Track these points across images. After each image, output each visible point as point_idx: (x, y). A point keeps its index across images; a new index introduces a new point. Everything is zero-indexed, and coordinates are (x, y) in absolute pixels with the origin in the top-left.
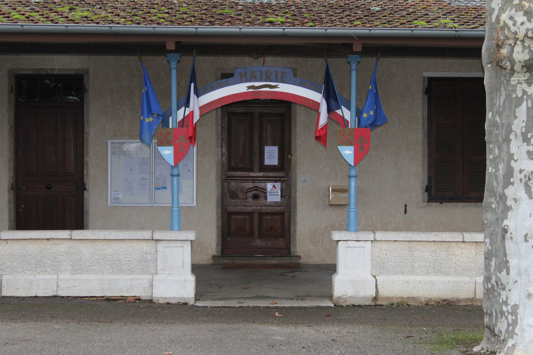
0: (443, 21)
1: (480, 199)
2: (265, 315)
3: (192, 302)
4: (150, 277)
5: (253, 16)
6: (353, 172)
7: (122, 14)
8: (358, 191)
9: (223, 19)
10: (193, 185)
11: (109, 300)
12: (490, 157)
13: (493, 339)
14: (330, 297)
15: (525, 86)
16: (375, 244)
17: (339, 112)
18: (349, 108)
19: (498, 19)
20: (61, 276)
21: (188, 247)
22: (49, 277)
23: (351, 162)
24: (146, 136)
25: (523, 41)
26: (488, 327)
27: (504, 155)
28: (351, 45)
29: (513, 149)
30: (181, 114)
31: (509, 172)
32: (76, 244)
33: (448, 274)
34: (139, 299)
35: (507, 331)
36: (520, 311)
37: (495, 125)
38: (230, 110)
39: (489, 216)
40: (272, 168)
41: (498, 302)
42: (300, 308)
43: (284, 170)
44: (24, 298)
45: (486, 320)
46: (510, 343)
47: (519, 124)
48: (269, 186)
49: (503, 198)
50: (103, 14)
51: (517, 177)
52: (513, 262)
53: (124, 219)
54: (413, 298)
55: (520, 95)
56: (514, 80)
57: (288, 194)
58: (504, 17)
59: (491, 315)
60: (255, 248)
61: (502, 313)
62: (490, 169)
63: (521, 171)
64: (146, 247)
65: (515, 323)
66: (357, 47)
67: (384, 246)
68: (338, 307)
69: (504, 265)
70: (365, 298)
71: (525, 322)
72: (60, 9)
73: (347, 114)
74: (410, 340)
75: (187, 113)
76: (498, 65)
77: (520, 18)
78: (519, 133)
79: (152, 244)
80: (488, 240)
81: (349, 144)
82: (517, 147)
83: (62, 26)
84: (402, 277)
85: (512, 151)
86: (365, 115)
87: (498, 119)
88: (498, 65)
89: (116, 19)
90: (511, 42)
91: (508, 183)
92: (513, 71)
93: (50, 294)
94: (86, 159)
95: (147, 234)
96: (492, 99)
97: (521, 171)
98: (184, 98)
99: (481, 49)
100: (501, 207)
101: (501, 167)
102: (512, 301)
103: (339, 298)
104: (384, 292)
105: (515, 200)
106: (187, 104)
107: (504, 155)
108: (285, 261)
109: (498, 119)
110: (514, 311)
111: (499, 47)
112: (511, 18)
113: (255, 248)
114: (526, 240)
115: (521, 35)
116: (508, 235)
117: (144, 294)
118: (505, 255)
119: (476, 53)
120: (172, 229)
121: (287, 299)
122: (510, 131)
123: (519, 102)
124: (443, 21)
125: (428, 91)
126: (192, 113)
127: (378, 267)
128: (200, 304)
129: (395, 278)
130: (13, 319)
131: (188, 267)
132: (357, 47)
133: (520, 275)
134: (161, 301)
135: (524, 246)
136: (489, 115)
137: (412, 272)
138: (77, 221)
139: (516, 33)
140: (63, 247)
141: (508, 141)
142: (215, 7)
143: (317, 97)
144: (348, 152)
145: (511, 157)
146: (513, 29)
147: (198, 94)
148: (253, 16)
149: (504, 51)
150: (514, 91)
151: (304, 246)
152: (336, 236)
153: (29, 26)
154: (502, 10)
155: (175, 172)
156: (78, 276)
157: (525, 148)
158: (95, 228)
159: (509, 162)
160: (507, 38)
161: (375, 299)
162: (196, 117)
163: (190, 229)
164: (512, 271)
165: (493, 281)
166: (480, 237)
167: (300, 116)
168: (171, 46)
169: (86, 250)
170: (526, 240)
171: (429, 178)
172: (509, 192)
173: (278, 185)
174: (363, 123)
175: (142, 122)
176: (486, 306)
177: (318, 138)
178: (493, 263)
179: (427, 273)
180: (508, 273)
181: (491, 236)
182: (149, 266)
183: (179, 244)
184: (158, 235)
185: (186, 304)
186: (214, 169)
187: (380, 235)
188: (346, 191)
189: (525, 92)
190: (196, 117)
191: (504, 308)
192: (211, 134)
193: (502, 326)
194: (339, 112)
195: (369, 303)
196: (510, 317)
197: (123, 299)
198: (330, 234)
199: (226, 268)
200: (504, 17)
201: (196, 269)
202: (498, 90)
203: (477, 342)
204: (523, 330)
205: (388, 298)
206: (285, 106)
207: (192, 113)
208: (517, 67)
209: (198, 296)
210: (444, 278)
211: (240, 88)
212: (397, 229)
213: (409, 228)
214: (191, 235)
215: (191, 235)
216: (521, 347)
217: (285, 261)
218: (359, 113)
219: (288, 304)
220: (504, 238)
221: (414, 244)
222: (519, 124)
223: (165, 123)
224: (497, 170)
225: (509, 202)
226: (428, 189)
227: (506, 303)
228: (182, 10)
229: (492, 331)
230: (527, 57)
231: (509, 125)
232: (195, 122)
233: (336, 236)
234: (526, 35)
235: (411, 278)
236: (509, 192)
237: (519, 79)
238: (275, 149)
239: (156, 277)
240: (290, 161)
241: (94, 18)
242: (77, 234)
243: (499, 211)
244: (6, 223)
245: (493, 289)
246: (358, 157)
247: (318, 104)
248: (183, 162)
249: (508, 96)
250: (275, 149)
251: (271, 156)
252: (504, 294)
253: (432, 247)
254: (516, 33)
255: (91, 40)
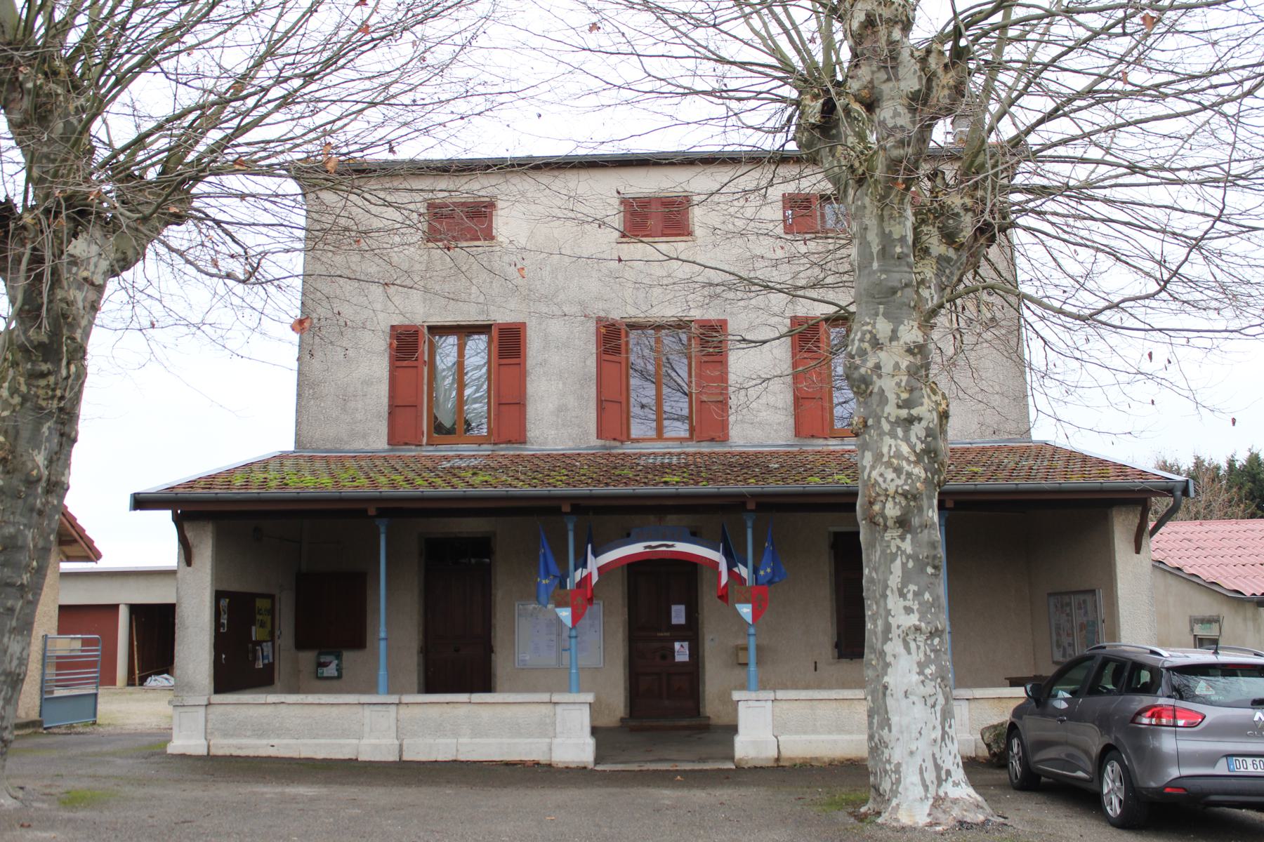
0: (836, 477)
1: (861, 655)
2: (665, 778)
3: (591, 766)
4: (548, 740)
5: (650, 476)
6: (752, 631)
7: (522, 477)
8: (759, 649)
9: (619, 480)
10: (600, 647)
11: (508, 764)
12: (868, 613)
13: (879, 799)
14: (732, 758)
15: (898, 541)
16: (776, 703)
17: (736, 570)
18: (746, 566)
19: (869, 477)
20: (461, 740)
21: (586, 710)
22: (449, 741)
23: (750, 621)
24: (543, 598)
25: (894, 498)
26: (874, 787)
27: (882, 612)
28: (744, 504)
29: (890, 605)
30: (579, 575)
31: (888, 629)
32: (476, 707)
33: (851, 733)
34: (538, 764)
35: (891, 790)
36: (903, 769)
37: (872, 581)
38: (634, 567)
39: (870, 673)
40: (679, 627)
41: (881, 760)
42: (700, 771)
43: (691, 632)
44: (424, 763)
45: (872, 779)
46: (894, 802)
47: (895, 580)
48: (677, 645)
49: (882, 654)
50: (504, 478)
51: (895, 632)
52: (894, 719)
53: (531, 681)
54: (817, 759)
55: (894, 550)
56: (888, 536)
57: (695, 652)
58: (875, 474)
59: (875, 774)
60: (664, 710)
61: (886, 772)
62: (869, 626)
63: (898, 627)
64: (545, 709)
65: (898, 781)
66: (751, 505)
67: (785, 705)
68: (739, 768)
69: (886, 723)
70: (767, 759)
71: (908, 780)
72: (463, 474)
73: (743, 571)
74: (801, 802)
75: (585, 573)
76: (872, 522)
77: (890, 475)
78: (895, 589)
79: (550, 707)
80: (869, 698)
81: (747, 602)
82: (894, 603)
83: (461, 489)
84: (804, 737)
85: (890, 606)
86: (762, 573)
87: (874, 575)
88: (872, 522)
89: (515, 483)
90: (883, 498)
91: (886, 639)
92: (886, 528)
93: (449, 757)
94: (493, 621)
95: (545, 697)
96: (868, 555)
97: (898, 627)
98: (581, 561)
99: (855, 504)
100: (881, 663)
101: (880, 623)
102: (895, 760)
103: (741, 759)
104: (787, 752)
105: (894, 656)
106: (584, 565)
107: (882, 612)
108: (694, 722)
109: (874, 575)
110: (897, 770)
111: (871, 503)
112: (881, 475)
113: (664, 710)
114: (906, 696)
115: (891, 491)
116: (888, 692)
117: (542, 758)
118: (887, 712)
119: (852, 507)
120: (570, 691)
121: (689, 761)
122: (887, 587)
123: (893, 557)
124: (836, 477)
125: (834, 546)
126: (590, 574)
127: (779, 727)
128: (599, 768)
129: (797, 737)
130: (407, 784)
131: (587, 730)
132: (751, 505)
133: (902, 732)
134: (560, 765)
135: (904, 702)
136: (866, 571)
137: (815, 731)
138: (485, 684)
139: (886, 490)
140: (462, 711)
141: (885, 596)
142: (615, 468)
143: (715, 556)
144: (746, 610)
145: (888, 612)
146: (884, 486)
147: (596, 554)
148: (650, 476)
149: (877, 508)
150: (888, 546)
151: (712, 707)
152: (736, 695)
153: (428, 491)
154: (873, 467)
155: (574, 633)
156: (478, 740)
157: (902, 603)
158: (502, 691)
159: (886, 618)
160: (878, 495)
161: (778, 760)
162: (595, 579)
163: (589, 691)
164: (894, 729)
165: (876, 739)
166: (859, 693)
167: (706, 575)
168: (566, 508)
169: (485, 714)
170: (906, 696)
171: (839, 635)
172: (888, 648)
173: (686, 644)
174: (760, 581)
175: (538, 584)
176: (870, 764)
177: (720, 597)
178: (875, 721)
179: (830, 733)
180: (890, 731)
181: (873, 693)
182: (547, 729)
183: (577, 707)
184: (556, 698)
185: (585, 768)
186: (621, 630)
187: (780, 694)
188: (746, 649)
189: (899, 548)
190: (595, 579)
191: (888, 767)
192: (618, 594)
193: (886, 786)
194: (736, 570)
195: (771, 764)
196: (893, 776)
197: (522, 763)
198: (730, 695)
199: (633, 730)
200: (875, 474)
201: (595, 731)
202: (874, 546)
203: (865, 802)
204: (906, 789)
205: (791, 759)
206: (691, 566)
207: (590, 574)
208: (890, 523)
209: (598, 760)
210: (847, 737)
211: (637, 548)
212: (807, 687)
213: (819, 686)
214: (590, 698)
215: (590, 698)
216: (904, 806)
217: (694, 722)
218: (755, 571)
219: (688, 767)
220: (884, 694)
221: (815, 703)
222: (895, 580)
223: (563, 585)
224: (876, 626)
225: (889, 659)
226: (837, 646)
227: (889, 761)
228: (582, 472)
229: (877, 790)
230: (899, 513)
231: (886, 581)
232: (594, 582)
233: (736, 695)
234: (896, 492)
235: (813, 737)
236: (888, 648)
237: (892, 534)
238: (682, 608)
239: (557, 741)
240: (697, 619)
241: (493, 482)
242: (477, 697)
243: (879, 668)
244: (416, 687)
245: (877, 747)
246: (756, 615)
247: (717, 563)
248: (581, 622)
249: (883, 552)
250: (682, 608)
251: (678, 615)
252: (887, 752)
253: (834, 704)
254: (886, 490)
255: (547, 503)
